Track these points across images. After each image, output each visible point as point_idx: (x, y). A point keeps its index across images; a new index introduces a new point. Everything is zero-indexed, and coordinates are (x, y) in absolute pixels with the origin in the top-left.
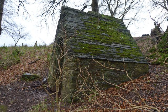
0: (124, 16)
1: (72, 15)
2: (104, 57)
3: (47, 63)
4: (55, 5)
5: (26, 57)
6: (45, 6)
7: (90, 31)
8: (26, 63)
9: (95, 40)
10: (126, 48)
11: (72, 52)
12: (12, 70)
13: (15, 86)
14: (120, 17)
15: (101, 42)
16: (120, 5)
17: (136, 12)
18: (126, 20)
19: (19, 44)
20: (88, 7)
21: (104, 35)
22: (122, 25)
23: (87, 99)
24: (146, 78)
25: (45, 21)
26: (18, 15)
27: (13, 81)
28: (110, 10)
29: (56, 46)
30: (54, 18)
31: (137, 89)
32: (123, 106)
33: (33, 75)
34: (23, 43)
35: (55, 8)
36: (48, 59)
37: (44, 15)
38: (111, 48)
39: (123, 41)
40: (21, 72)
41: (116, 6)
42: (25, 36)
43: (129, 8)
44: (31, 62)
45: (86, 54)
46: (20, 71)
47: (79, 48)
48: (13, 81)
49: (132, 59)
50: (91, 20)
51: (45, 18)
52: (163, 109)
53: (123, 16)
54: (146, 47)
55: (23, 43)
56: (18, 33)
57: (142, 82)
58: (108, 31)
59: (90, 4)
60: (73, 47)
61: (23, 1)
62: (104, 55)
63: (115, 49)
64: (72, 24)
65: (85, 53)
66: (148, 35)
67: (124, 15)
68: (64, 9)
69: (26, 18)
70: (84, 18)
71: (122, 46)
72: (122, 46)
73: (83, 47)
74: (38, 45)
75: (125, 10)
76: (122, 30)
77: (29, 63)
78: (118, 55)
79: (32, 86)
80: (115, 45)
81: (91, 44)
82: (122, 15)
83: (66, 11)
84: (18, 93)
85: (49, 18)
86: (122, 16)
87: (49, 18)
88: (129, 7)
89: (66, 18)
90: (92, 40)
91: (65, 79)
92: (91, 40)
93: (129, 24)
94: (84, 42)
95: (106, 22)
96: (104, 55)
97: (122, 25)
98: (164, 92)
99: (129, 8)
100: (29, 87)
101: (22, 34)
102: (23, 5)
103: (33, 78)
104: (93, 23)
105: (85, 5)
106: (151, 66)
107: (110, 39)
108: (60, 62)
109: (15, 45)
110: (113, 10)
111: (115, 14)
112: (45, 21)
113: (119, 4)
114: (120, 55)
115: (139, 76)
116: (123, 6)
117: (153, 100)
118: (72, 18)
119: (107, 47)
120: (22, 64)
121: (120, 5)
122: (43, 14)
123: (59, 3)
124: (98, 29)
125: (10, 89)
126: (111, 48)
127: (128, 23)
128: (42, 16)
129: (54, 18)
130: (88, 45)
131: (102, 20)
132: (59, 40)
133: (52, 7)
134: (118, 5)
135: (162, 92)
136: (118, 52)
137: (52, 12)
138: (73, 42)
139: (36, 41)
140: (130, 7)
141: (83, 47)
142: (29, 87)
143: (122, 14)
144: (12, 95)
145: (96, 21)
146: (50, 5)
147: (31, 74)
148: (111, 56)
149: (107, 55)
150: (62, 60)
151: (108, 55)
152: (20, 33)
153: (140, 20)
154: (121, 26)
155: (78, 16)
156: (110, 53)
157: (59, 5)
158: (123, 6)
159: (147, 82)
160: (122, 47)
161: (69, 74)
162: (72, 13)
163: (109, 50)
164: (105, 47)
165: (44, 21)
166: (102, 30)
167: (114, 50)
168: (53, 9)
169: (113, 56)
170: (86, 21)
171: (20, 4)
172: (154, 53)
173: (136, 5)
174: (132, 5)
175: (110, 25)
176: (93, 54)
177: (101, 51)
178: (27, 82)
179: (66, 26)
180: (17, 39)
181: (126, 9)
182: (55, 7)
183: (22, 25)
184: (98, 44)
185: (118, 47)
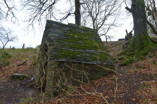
0: (104, 21)
1: (55, 27)
2: (80, 60)
3: (34, 65)
4: (41, 12)
5: (15, 60)
6: (32, 13)
7: (69, 40)
8: (15, 65)
9: (73, 47)
10: (97, 53)
11: (54, 57)
12: (2, 71)
13: (6, 84)
14: (101, 22)
15: (78, 49)
16: (101, 12)
17: (115, 18)
18: (106, 25)
19: (8, 46)
20: (71, 14)
21: (80, 43)
22: (96, 34)
23: (65, 93)
24: (112, 76)
25: (32, 26)
26: (6, 20)
27: (4, 80)
28: (92, 16)
29: (41, 54)
30: (40, 23)
31: (104, 85)
32: (91, 96)
33: (22, 76)
34: (10, 46)
35: (42, 15)
36: (34, 61)
37: (32, 20)
38: (86, 53)
39: (96, 47)
40: (11, 72)
41: (97, 13)
42: (13, 39)
43: (109, 15)
44: (20, 64)
45: (65, 58)
46: (10, 72)
47: (60, 53)
48: (4, 80)
49: (102, 62)
50: (71, 30)
51: (33, 23)
52: (118, 97)
53: (104, 22)
54: (118, 51)
55: (10, 46)
56: (6, 36)
57: (109, 80)
58: (84, 39)
59: (73, 12)
60: (55, 53)
61: (11, 8)
62: (79, 59)
63: (88, 54)
64: (53, 35)
65: (64, 58)
66: (123, 39)
67: (104, 21)
68: (48, 23)
69: (14, 22)
70: (64, 30)
71: (95, 52)
72: (95, 52)
73: (63, 53)
74: (25, 47)
75: (105, 17)
76: (95, 38)
77: (17, 65)
78: (91, 59)
79: (21, 85)
80: (88, 51)
81: (70, 51)
82: (102, 21)
83: (50, 24)
84: (9, 91)
85: (36, 23)
86: (102, 22)
87: (36, 23)
88: (109, 14)
89: (51, 29)
90: (70, 47)
91: (49, 78)
92: (69, 47)
93: (109, 29)
94: (63, 49)
95: (83, 32)
96: (79, 59)
97: (96, 34)
98: (122, 86)
99: (109, 15)
100: (19, 85)
101: (10, 37)
102: (11, 11)
103: (22, 78)
104: (72, 34)
105: (68, 13)
106: (119, 66)
107: (85, 46)
108: (44, 66)
109: (4, 47)
110: (95, 16)
111: (97, 19)
112: (32, 26)
113: (100, 11)
114: (92, 59)
115: (107, 75)
116: (104, 13)
117: (112, 92)
118: (55, 29)
119: (82, 53)
120: (11, 65)
121: (101, 12)
122: (30, 20)
123: (45, 10)
124: (76, 38)
125: (2, 87)
126: (86, 53)
127: (108, 28)
128: (29, 21)
129: (40, 23)
130: (67, 51)
131: (79, 30)
132: (44, 47)
133: (39, 14)
134: (99, 12)
135: (121, 86)
136: (90, 56)
137: (39, 18)
138: (55, 49)
139: (24, 44)
140: (110, 14)
141: (63, 53)
142: (19, 85)
143: (102, 20)
144: (5, 92)
145: (74, 31)
146: (37, 12)
147: (20, 75)
148: (85, 60)
149: (82, 59)
150: (46, 63)
151: (83, 59)
152: (8, 36)
153: (119, 25)
154: (95, 35)
155: (60, 28)
156: (84, 57)
157: (45, 11)
158: (104, 13)
159: (112, 79)
160: (94, 52)
161: (52, 74)
162: (55, 25)
163: (84, 55)
164: (81, 52)
165: (31, 26)
166: (79, 39)
167: (88, 55)
168: (40, 15)
169: (86, 60)
170: (66, 31)
171: (9, 10)
172: (123, 56)
173: (114, 13)
174: (111, 12)
175: (85, 35)
176: (71, 58)
177: (77, 56)
178: (17, 81)
179: (50, 36)
180: (5, 42)
181: (106, 15)
182: (41, 13)
183: (10, 29)
184: (75, 50)
185: (91, 52)
